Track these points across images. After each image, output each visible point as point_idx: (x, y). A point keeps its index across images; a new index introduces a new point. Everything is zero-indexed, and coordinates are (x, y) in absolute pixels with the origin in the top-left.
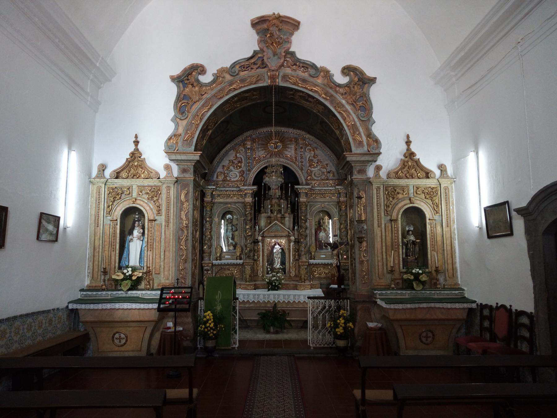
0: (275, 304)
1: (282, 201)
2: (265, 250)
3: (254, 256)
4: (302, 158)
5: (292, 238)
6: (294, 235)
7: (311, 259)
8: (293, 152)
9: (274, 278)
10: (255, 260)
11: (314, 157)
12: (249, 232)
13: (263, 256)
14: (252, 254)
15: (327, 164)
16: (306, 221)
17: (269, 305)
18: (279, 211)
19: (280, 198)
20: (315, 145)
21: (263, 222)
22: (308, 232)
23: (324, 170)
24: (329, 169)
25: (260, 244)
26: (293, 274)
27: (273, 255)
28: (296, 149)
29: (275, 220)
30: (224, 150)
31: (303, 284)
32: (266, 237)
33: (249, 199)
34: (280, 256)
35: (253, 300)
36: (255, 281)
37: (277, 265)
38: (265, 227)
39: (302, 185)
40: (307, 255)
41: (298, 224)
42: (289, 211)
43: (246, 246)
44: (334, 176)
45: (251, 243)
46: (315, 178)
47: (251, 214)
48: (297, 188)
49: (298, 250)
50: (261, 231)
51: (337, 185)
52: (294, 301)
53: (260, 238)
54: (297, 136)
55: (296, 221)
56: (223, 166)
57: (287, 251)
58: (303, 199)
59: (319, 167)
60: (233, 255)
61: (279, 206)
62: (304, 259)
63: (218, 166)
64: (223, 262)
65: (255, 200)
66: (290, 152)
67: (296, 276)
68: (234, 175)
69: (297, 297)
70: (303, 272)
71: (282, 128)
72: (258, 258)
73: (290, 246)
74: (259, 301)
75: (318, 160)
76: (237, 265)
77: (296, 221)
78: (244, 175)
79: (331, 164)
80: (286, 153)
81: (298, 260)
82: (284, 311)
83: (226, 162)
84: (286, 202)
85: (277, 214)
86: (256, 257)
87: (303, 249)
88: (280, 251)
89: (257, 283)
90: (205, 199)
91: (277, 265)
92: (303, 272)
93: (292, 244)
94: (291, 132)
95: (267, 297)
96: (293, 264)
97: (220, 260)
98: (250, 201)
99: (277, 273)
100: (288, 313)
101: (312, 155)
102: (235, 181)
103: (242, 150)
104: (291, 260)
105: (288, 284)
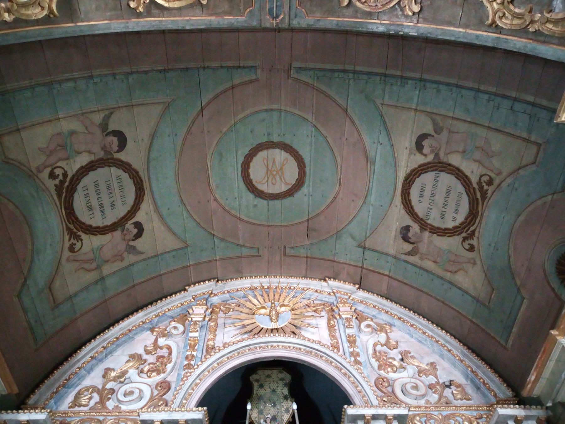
24: (444, 378)
28: (331, 328)
54: (332, 299)
59: (411, 370)
63: (89, 372)
75: (401, 353)
83: (118, 361)
103: (175, 328)
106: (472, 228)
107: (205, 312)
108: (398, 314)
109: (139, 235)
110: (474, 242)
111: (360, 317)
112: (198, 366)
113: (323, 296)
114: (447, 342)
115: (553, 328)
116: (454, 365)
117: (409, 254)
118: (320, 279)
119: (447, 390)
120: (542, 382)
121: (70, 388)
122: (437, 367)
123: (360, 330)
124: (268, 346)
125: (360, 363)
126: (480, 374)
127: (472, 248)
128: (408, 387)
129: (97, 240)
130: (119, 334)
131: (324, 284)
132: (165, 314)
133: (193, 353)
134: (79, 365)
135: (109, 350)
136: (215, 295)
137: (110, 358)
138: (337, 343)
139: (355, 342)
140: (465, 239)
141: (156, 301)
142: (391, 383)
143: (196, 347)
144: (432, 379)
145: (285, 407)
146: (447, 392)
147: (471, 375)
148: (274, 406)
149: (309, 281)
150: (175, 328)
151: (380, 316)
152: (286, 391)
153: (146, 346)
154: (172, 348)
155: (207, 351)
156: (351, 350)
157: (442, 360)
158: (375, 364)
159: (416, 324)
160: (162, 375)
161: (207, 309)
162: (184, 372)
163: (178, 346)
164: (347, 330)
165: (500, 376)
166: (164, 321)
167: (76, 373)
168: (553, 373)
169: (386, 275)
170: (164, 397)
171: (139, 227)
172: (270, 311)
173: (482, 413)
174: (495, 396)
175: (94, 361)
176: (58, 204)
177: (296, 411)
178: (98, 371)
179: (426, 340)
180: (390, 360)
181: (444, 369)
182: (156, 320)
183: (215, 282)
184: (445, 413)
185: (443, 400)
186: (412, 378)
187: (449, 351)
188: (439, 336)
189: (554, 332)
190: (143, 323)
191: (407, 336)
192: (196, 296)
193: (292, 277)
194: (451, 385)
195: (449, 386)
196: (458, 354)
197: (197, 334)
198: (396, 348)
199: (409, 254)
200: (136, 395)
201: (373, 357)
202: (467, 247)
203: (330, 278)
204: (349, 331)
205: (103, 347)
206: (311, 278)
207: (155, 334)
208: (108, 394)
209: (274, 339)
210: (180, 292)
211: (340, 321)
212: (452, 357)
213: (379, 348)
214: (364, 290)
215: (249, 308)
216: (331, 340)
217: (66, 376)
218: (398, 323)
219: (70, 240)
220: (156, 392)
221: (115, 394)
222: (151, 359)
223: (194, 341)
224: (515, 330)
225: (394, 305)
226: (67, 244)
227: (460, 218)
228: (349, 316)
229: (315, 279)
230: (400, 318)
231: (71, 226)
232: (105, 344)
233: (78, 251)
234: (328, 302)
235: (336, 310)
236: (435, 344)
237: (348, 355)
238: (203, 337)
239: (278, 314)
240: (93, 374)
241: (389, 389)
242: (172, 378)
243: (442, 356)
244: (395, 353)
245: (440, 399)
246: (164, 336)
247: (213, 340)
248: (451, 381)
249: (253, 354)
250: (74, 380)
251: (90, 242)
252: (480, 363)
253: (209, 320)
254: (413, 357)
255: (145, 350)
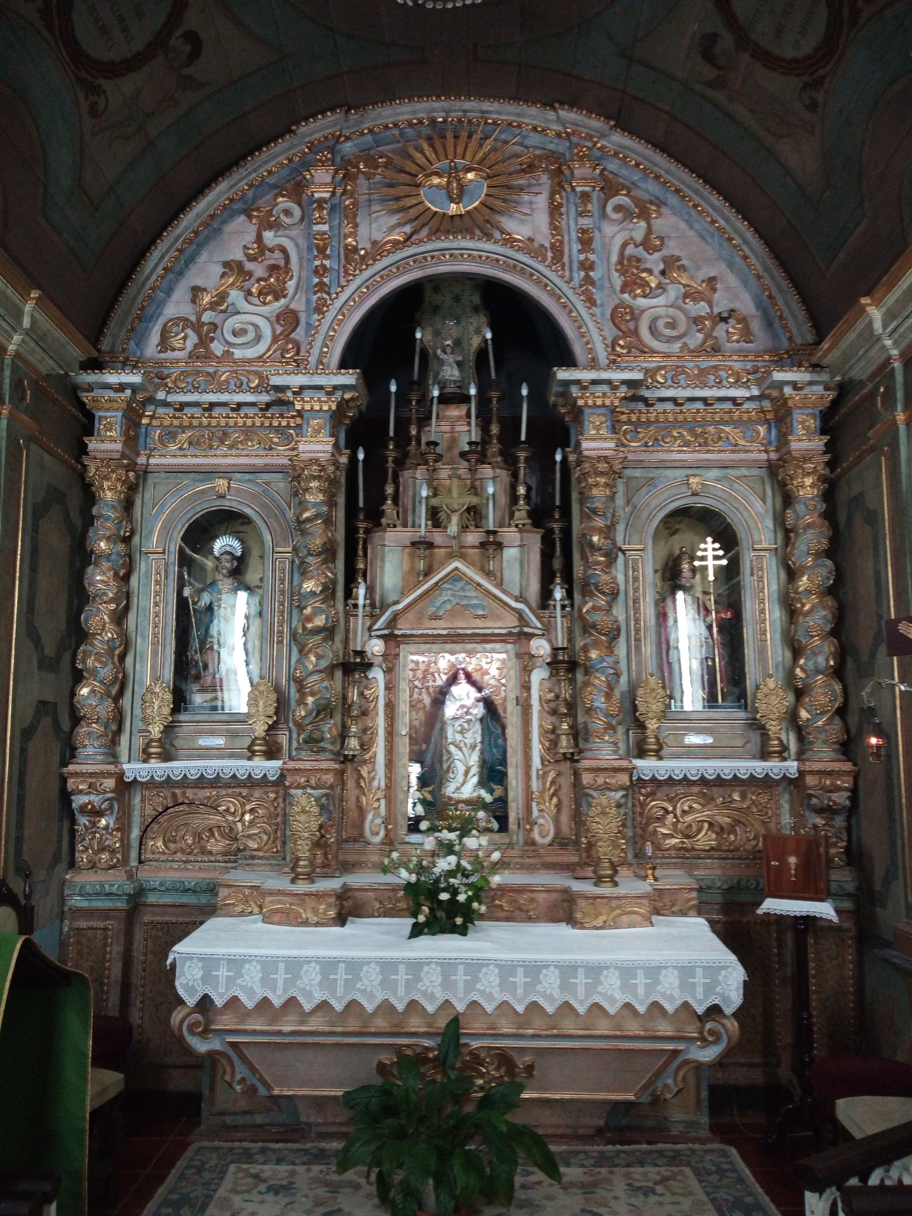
0: (455, 1022)
1: (487, 471)
2: (403, 707)
3: (343, 736)
4: (586, 242)
5: (541, 647)
6: (547, 631)
7: (642, 753)
8: (542, 219)
9: (445, 864)
10: (347, 759)
11: (646, 243)
12: (316, 612)
13: (390, 734)
14: (329, 728)
15: (711, 281)
16: (611, 557)
17: (415, 1024)
18: (474, 514)
19: (478, 454)
20: (652, 187)
21: (390, 565)
22: (619, 612)
23: (702, 308)
24: (722, 303)
25: (377, 675)
26: (544, 830)
27: (443, 730)
28: (554, 210)
29: (451, 556)
30: (201, 207)
31: (606, 890)
32: (408, 638)
33: (318, 445)
34: (475, 735)
35: (319, 996)
36: (346, 867)
37: (464, 785)
38: (403, 594)
39: (593, 364)
40: (621, 730)
41: (568, 580)
42: (521, 515)
43: (300, 684)
44: (747, 334)
45: (330, 671)
46: (655, 344)
47: (328, 521)
48: (567, 383)
49: (571, 706)
50: (384, 607)
51: (780, 363)
52: (567, 1005)
53: (376, 647)
54: (561, 147)
55: (559, 564)
56: (196, 291)
57: (512, 717)
58: (595, 442)
59: (673, 292)
60: (234, 735)
61: (475, 489)
62: (605, 751)
63: (169, 291)
64: (178, 768)
65: (353, 459)
66: (529, 221)
67: (560, 841)
68: (250, 326)
69: (581, 979)
70: (605, 824)
71: (486, 106)
72: (365, 746)
73: (527, 687)
74: (353, 1006)
75: (665, 260)
76: (251, 783)
77: (557, 564)
78: (299, 334)
79: (732, 280)
80: (509, 224)
81: (571, 758)
82: (504, 1059)
83: (207, 272)
84: (504, 475)
85: (464, 528)
86: (353, 743)
87: (600, 702)
88: (479, 711)
89: (356, 880)
90: (93, 445)
91: (464, 785)
92: (605, 824)
93: (538, 676)
94: (538, 124)
95: (402, 976)
96: (542, 777)
97: (166, 756)
98: (324, 457)
99: (465, 832)
100: (530, 1068)
101: (639, 236)
102: (249, 361)
103: (287, 213)
104: (536, 762)
105: (520, 890)
106: (822, 72)
107: (333, 177)
108: (677, 183)
109: (195, 54)
110: (820, 97)
111: (610, 188)
112: (337, 294)
113: (548, 139)
114: (746, 242)
115: (867, 294)
116: (745, 283)
117: (710, 84)
118: (544, 105)
119: (722, 326)
120: (836, 354)
121: (150, 321)
122: (718, 286)
123: (604, 215)
124: (444, 256)
125: (593, 283)
126: (780, 301)
127: (813, 107)
128: (660, 323)
129: (128, 85)
130: (196, 225)
131: (551, 115)
132: (263, 181)
133: (325, 262)
134: (150, 283)
135: (188, 253)
136: (348, 138)
137: (194, 269)
138: (561, 242)
139: (591, 240)
140: (806, 86)
141: (244, 158)
142: (635, 315)
143: (328, 252)
144: (702, 308)
145: (475, 325)
146: (720, 331)
147: (766, 302)
148: (458, 323)
149: (523, 108)
150: (287, 213)
151: (643, 185)
152: (476, 299)
153: (245, 247)
154: (289, 250)
155: (346, 256)
156: (582, 257)
157: (730, 273)
158: (617, 280)
159: (703, 204)
160: (283, 301)
161: (336, 172)
162: (315, 297)
163: (297, 245)
164: (580, 219)
165: (808, 310)
166: (264, 195)
167: (149, 297)
168: (850, 345)
169: (667, 113)
170: (292, 336)
171: (192, 38)
172: (449, 183)
173: (760, 364)
174: (790, 339)
175: (171, 276)
176: (52, 43)
177: (490, 342)
178: (181, 293)
179: (712, 237)
180: (644, 275)
181: (727, 289)
182: (250, 194)
183: (343, 115)
184: (704, 365)
185: (710, 342)
186: (671, 306)
187: (745, 258)
188: (736, 231)
189: (864, 301)
190: (231, 200)
191: (683, 225)
192: (312, 143)
193: (489, 98)
194: (729, 318)
195: (725, 320)
196: (757, 264)
197: (325, 228)
198: (660, 250)
199: (710, 84)
200: (251, 335)
201: (617, 270)
202: (807, 101)
203: (562, 103)
204: (585, 222)
205: (178, 250)
206: (526, 101)
207: (254, 221)
208: (209, 332)
209: (455, 245)
210: (282, 136)
211: (571, 196)
212: (746, 270)
213: (630, 250)
214: (623, 129)
215: (410, 174)
216: (552, 235)
217: (138, 304)
218: (673, 200)
219: (87, 97)
220: (279, 329)
221: (219, 331)
222: (258, 270)
223: (322, 240)
224: (841, 256)
225: (673, 166)
226: (85, 108)
227: (808, 45)
228: (587, 189)
229: (534, 103)
230: (678, 191)
231: (84, 75)
232: (178, 245)
233: (104, 112)
234: (554, 152)
235: (567, 172)
236: (726, 244)
237: (575, 265)
238: (336, 232)
239: (461, 187)
240: (175, 296)
241: (631, 325)
242: (299, 305)
243: (731, 265)
244: (654, 261)
245: (704, 341)
246: (270, 227)
247: (354, 234)
248: (732, 310)
249: (421, 268)
250: (150, 310)
251: (119, 92)
252: (785, 284)
253: (342, 194)
254: (683, 268)
255: (247, 255)
